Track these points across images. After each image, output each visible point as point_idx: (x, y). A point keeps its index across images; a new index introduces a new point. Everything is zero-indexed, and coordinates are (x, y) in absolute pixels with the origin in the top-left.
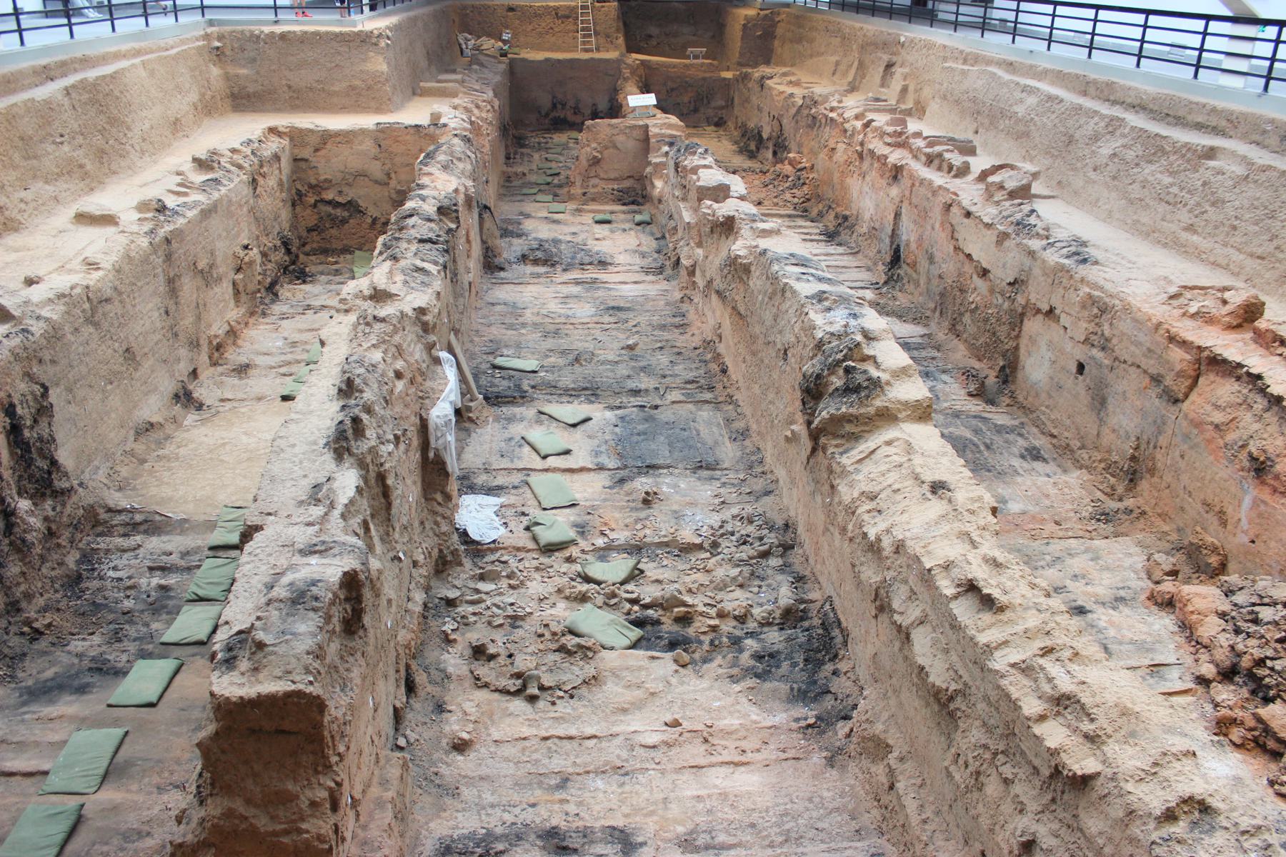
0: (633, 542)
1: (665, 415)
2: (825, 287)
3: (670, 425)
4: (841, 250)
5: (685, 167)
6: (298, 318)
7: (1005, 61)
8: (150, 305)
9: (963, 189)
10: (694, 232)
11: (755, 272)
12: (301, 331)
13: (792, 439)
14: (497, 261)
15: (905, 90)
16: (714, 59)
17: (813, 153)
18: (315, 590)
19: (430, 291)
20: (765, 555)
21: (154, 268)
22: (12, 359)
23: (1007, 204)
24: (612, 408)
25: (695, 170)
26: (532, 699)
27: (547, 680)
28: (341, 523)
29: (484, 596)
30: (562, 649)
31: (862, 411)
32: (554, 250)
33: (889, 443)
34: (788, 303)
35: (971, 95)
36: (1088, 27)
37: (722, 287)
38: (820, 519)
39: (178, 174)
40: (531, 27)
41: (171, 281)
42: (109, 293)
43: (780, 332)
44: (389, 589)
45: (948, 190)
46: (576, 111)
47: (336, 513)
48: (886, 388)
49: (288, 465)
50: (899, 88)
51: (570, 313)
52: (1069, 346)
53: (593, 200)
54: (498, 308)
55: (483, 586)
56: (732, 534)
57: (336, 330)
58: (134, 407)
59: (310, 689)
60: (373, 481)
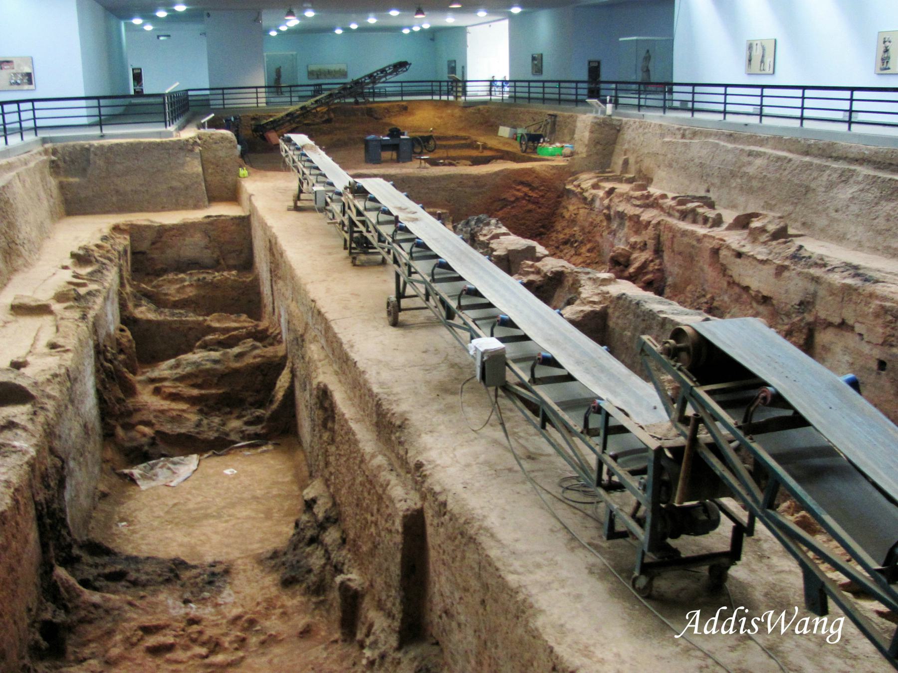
36: (757, 101)
45: (713, 238)
52: (866, 349)
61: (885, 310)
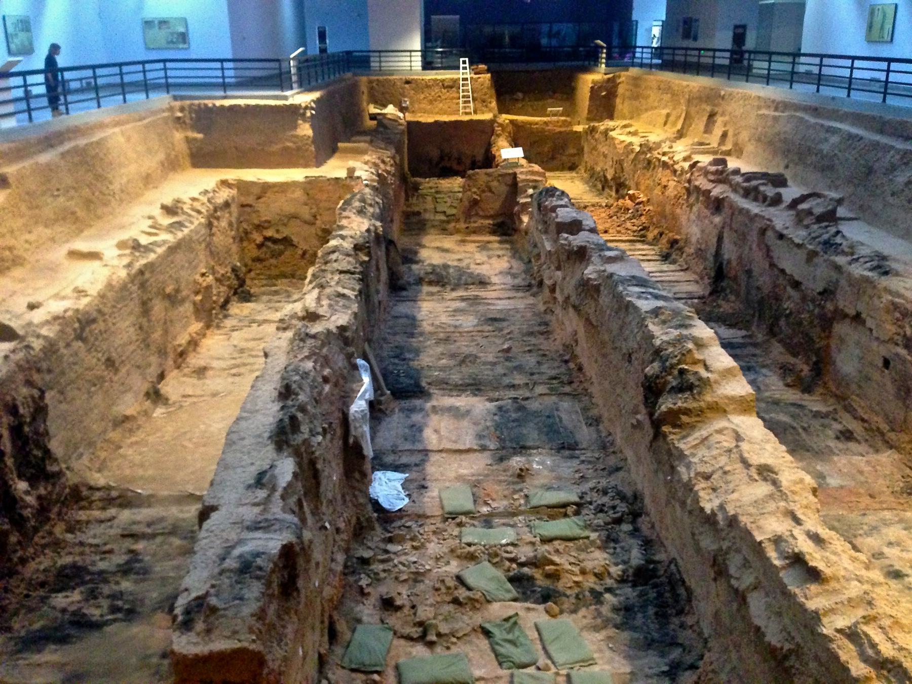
0: (510, 510)
1: (534, 405)
2: (660, 303)
3: (536, 414)
4: (672, 267)
5: (546, 207)
6: (245, 329)
7: (810, 107)
8: (127, 323)
9: (775, 216)
10: (554, 258)
11: (604, 291)
12: (247, 340)
13: (638, 426)
14: (401, 282)
15: (724, 135)
16: (568, 116)
17: (649, 189)
18: (259, 561)
19: (350, 312)
20: (618, 521)
21: (131, 293)
22: (17, 369)
23: (815, 227)
24: (491, 400)
25: (554, 209)
26: (431, 645)
27: (444, 628)
28: (280, 503)
29: (392, 556)
30: (456, 601)
31: (695, 405)
32: (444, 273)
33: (719, 431)
34: (630, 318)
35: (782, 136)
37: (577, 303)
38: (662, 492)
39: (150, 218)
40: (422, 96)
41: (144, 303)
42: (95, 314)
43: (625, 340)
44: (317, 555)
45: (763, 217)
46: (459, 161)
47: (277, 494)
48: (715, 386)
49: (239, 455)
50: (720, 133)
51: (458, 323)
53: (474, 232)
54: (402, 321)
55: (391, 547)
56: (590, 503)
57: (276, 344)
58: (113, 404)
59: (253, 647)
60: (305, 467)
61: (896, 306)
